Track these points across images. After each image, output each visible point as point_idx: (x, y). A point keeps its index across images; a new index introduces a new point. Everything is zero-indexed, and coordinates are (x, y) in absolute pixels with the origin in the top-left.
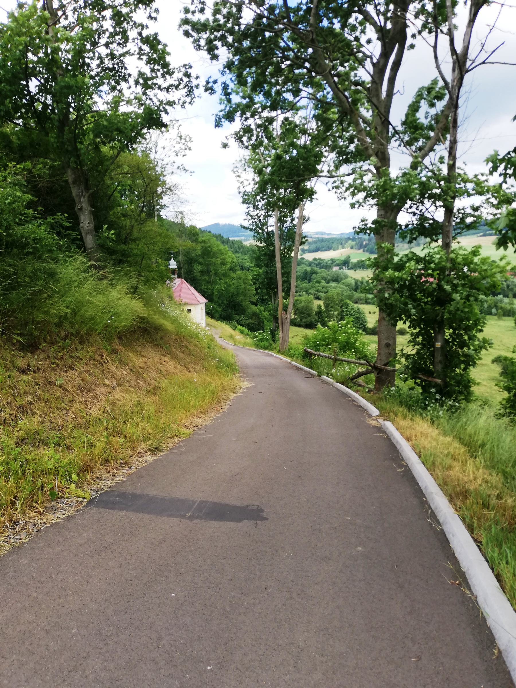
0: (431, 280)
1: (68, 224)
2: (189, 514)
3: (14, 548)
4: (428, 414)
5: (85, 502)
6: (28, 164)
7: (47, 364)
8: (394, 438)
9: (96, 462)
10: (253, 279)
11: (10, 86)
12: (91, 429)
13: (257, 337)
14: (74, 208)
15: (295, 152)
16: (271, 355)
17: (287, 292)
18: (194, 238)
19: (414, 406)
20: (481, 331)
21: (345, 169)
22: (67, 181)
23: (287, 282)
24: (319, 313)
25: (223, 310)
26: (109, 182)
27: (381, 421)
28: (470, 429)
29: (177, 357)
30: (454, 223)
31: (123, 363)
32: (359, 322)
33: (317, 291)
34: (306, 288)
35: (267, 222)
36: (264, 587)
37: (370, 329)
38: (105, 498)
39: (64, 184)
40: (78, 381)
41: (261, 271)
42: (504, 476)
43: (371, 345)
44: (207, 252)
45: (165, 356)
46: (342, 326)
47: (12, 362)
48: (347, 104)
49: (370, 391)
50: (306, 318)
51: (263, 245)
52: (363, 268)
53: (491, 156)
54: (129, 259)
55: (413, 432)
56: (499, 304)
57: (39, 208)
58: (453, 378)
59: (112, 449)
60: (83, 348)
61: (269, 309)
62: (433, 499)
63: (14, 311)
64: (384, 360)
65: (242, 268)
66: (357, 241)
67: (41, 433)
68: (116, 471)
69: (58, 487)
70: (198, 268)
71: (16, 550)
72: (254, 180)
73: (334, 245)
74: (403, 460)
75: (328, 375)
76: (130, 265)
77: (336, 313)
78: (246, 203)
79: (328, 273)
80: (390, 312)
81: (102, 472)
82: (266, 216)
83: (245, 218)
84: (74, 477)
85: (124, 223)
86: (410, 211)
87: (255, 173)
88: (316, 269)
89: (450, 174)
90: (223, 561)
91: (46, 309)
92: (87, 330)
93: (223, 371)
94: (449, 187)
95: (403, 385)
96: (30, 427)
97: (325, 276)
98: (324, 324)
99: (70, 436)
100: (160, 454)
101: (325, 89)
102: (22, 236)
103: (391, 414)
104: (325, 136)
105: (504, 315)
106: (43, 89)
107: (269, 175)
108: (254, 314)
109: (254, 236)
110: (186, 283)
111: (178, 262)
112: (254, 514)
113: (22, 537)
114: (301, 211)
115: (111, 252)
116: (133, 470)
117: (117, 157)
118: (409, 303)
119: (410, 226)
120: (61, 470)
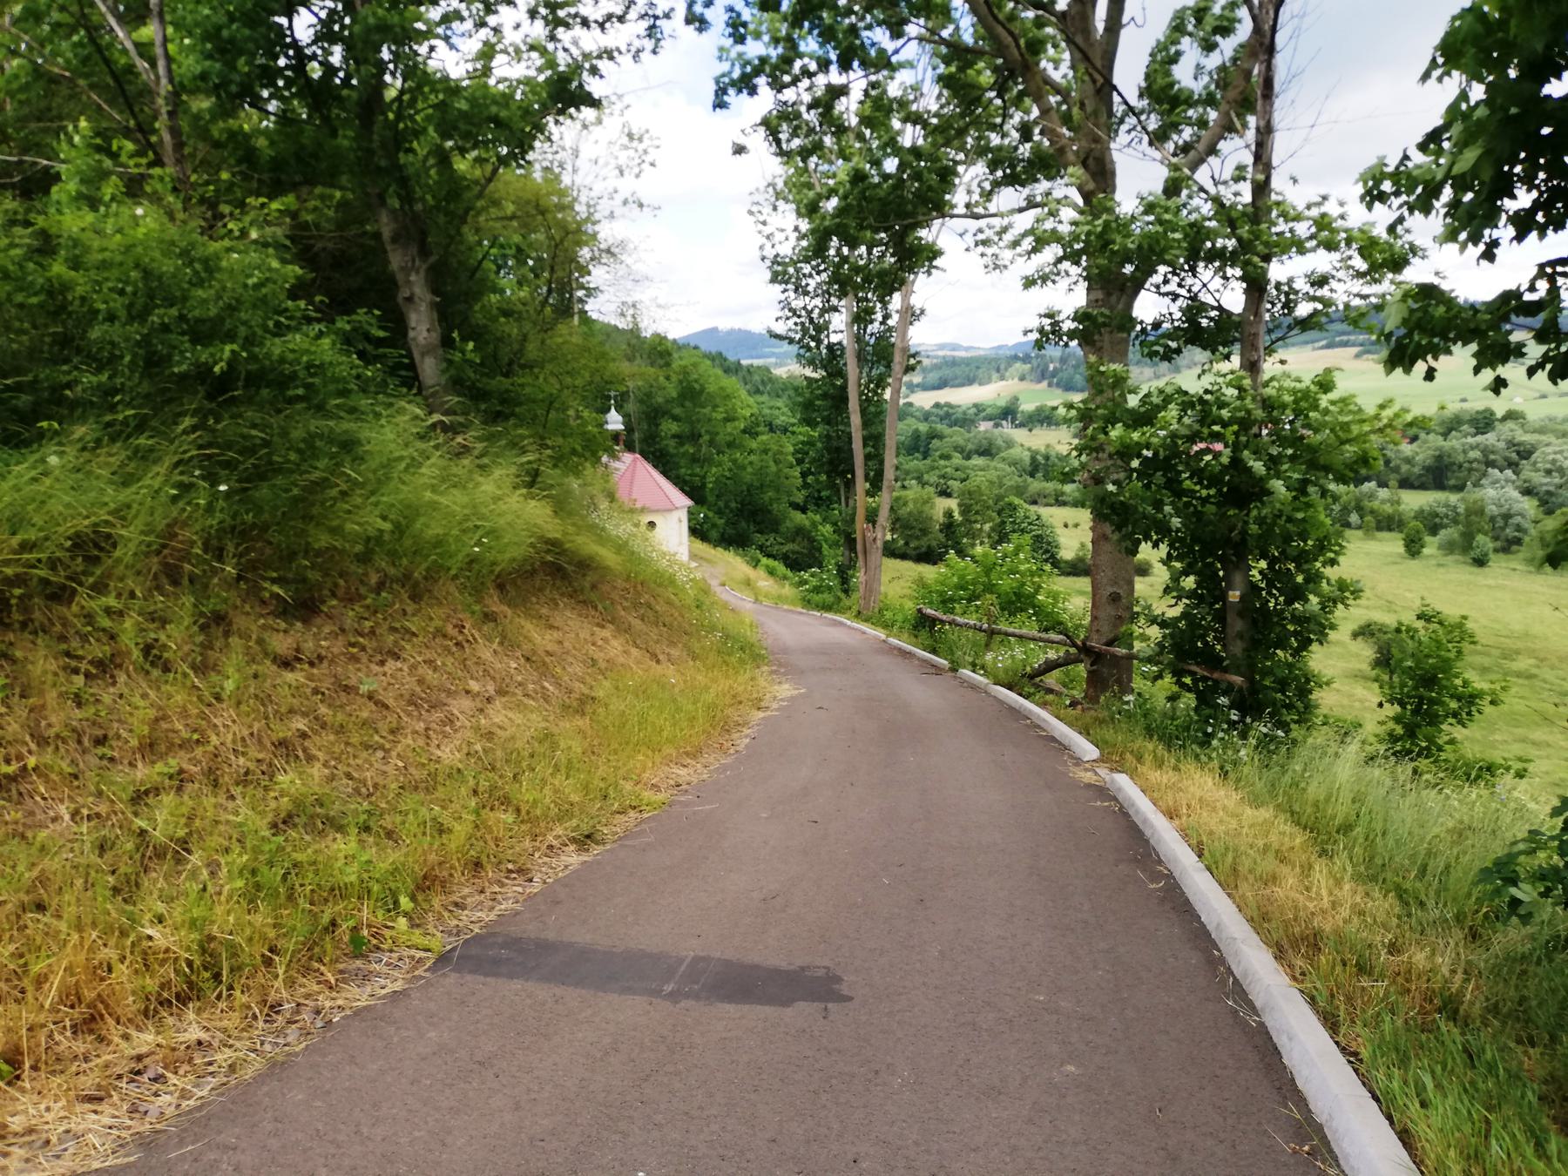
0: (1219, 447)
1: (381, 334)
2: (668, 988)
3: (273, 1064)
4: (1214, 755)
5: (431, 958)
6: (290, 200)
7: (338, 647)
8: (1137, 812)
9: (452, 867)
10: (797, 451)
11: (251, 28)
12: (440, 793)
13: (806, 582)
14: (394, 297)
16: (841, 624)
19: (1185, 737)
20: (1333, 562)
21: (1009, 197)
22: (377, 236)
23: (875, 458)
24: (949, 527)
25: (727, 524)
26: (472, 238)
27: (1103, 772)
28: (1314, 790)
29: (628, 630)
30: (1267, 317)
31: (508, 643)
32: (1045, 548)
33: (943, 477)
35: (828, 323)
36: (850, 1157)
37: (1066, 562)
38: (474, 951)
39: (373, 243)
40: (410, 684)
42: (1400, 897)
43: (1075, 600)
44: (691, 393)
45: (603, 627)
46: (1005, 556)
47: (260, 642)
48: (1015, 52)
49: (1073, 704)
50: (918, 538)
52: (1049, 424)
55: (1183, 799)
56: (1366, 504)
57: (318, 298)
59: (488, 837)
60: (419, 610)
61: (833, 519)
62: (1236, 953)
63: (265, 528)
64: (1107, 632)
65: (771, 428)
66: (1035, 363)
67: (327, 802)
68: (497, 889)
69: (369, 926)
70: (669, 427)
71: (277, 1068)
72: (796, 229)
74: (1160, 862)
75: (973, 667)
76: (522, 422)
77: (987, 527)
78: (780, 283)
79: (967, 435)
80: (1120, 522)
81: (466, 891)
82: (823, 311)
83: (780, 314)
84: (405, 902)
85: (507, 329)
86: (1164, 289)
87: (799, 214)
88: (939, 426)
89: (1260, 203)
90: (753, 1096)
91: (335, 523)
92: (428, 570)
94: (1250, 235)
95: (1155, 690)
96: (304, 790)
97: (961, 442)
98: (961, 553)
99: (394, 810)
100: (597, 850)
102: (282, 360)
103: (1128, 755)
105: (1379, 529)
106: (326, 34)
107: (834, 216)
108: (800, 532)
109: (799, 355)
110: (645, 463)
111: (626, 416)
112: (821, 988)
113: (289, 1039)
114: (906, 298)
115: (476, 395)
116: (536, 887)
117: (490, 180)
118: (1167, 500)
119: (1165, 325)
120: (376, 888)
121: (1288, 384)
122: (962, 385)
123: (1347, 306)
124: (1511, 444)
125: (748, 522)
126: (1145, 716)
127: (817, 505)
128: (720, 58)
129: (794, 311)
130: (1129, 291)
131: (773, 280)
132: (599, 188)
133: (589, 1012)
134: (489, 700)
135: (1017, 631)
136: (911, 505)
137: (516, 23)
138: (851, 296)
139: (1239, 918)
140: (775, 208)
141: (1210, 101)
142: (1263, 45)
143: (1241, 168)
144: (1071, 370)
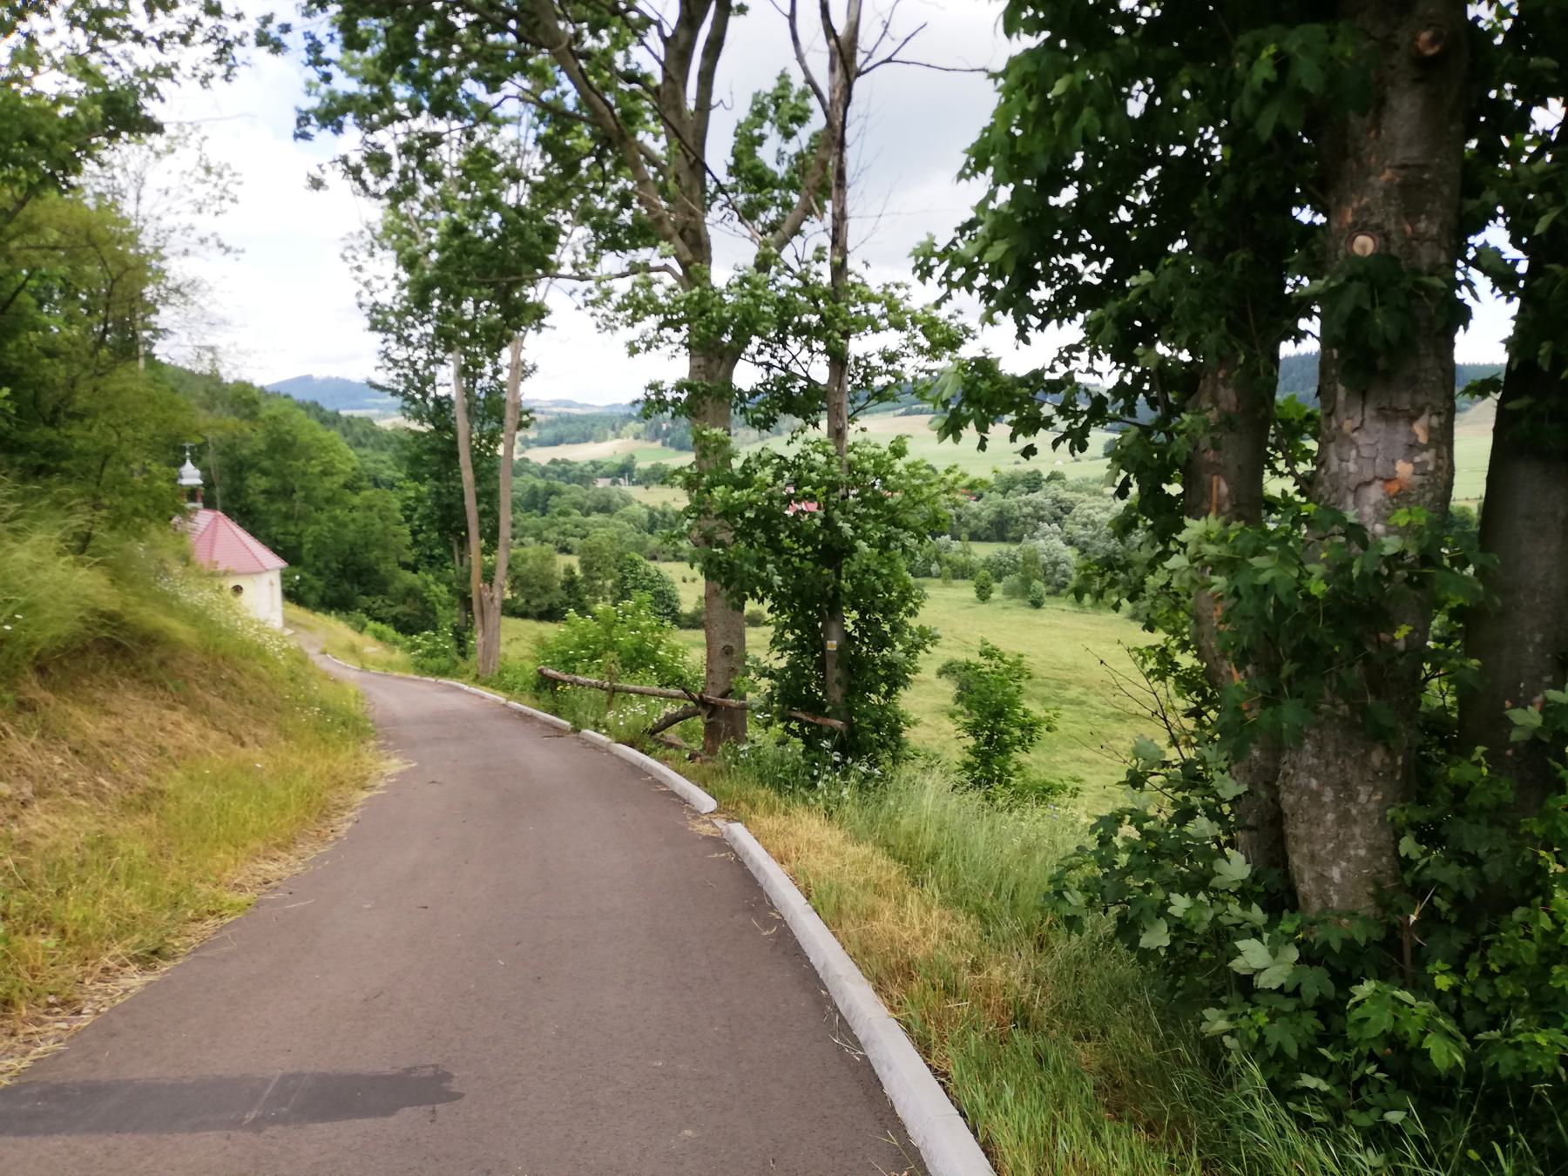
2: (250, 1116)
10: (406, 508)
13: (419, 646)
15: (495, 220)
16: (459, 689)
17: (492, 538)
18: (247, 411)
19: (793, 782)
20: (911, 613)
21: (611, 262)
23: (490, 515)
24: (570, 584)
25: (328, 585)
27: (720, 823)
28: (906, 823)
30: (849, 388)
31: (50, 735)
32: (665, 603)
33: (564, 533)
34: (536, 527)
35: (433, 375)
41: (424, 489)
43: (691, 651)
44: (282, 445)
45: (173, 709)
48: (611, 121)
50: (538, 596)
51: (427, 427)
53: (922, 245)
54: (64, 464)
56: (943, 555)
58: (866, 715)
59: (21, 968)
65: (377, 483)
68: (34, 1029)
72: (396, 277)
73: (596, 430)
74: (772, 908)
75: (596, 727)
76: (68, 475)
77: (609, 583)
78: (381, 331)
79: (586, 492)
80: (729, 582)
82: (429, 363)
85: (49, 373)
86: (759, 359)
89: (838, 284)
93: (333, 736)
94: (833, 312)
95: (762, 737)
97: (580, 499)
98: (583, 610)
100: (165, 966)
101: (558, 83)
103: (743, 805)
104: (562, 187)
105: (955, 577)
108: (411, 593)
110: (229, 521)
111: (205, 470)
112: (424, 1088)
114: (516, 353)
116: (87, 1018)
118: (769, 558)
121: (869, 450)
122: (578, 442)
123: (915, 379)
124: (1056, 501)
125: (351, 583)
126: (758, 764)
127: (431, 565)
128: (309, 93)
129: (395, 362)
130: (728, 359)
131: (373, 328)
132: (168, 222)
133: (151, 1159)
134: (24, 804)
135: (638, 688)
136: (530, 562)
137: (55, 32)
138: (458, 349)
139: (843, 955)
140: (372, 255)
141: (790, 185)
142: (834, 138)
143: (820, 250)
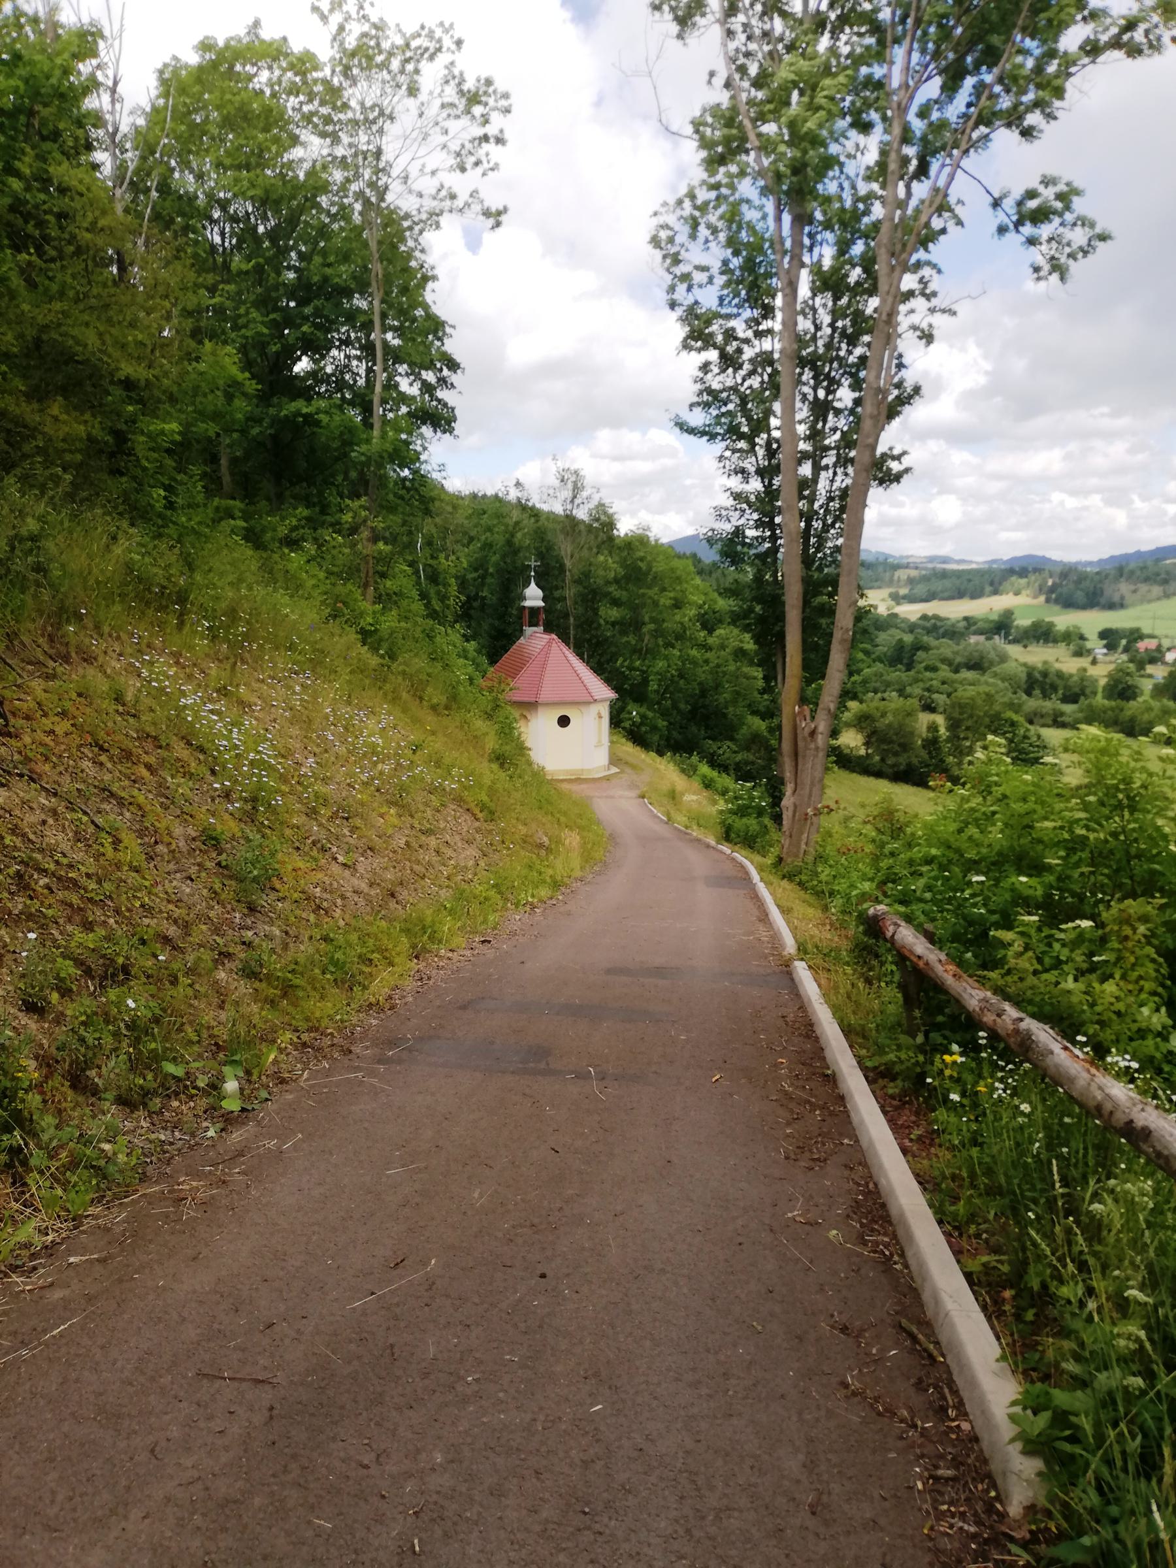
24: (932, 743)
33: (928, 690)
50: (896, 754)
52: (1046, 641)
79: (956, 648)
88: (925, 638)
97: (949, 655)
109: (721, 458)
122: (951, 598)
144: (1072, 586)
